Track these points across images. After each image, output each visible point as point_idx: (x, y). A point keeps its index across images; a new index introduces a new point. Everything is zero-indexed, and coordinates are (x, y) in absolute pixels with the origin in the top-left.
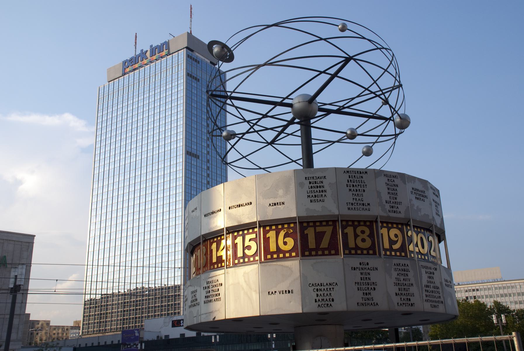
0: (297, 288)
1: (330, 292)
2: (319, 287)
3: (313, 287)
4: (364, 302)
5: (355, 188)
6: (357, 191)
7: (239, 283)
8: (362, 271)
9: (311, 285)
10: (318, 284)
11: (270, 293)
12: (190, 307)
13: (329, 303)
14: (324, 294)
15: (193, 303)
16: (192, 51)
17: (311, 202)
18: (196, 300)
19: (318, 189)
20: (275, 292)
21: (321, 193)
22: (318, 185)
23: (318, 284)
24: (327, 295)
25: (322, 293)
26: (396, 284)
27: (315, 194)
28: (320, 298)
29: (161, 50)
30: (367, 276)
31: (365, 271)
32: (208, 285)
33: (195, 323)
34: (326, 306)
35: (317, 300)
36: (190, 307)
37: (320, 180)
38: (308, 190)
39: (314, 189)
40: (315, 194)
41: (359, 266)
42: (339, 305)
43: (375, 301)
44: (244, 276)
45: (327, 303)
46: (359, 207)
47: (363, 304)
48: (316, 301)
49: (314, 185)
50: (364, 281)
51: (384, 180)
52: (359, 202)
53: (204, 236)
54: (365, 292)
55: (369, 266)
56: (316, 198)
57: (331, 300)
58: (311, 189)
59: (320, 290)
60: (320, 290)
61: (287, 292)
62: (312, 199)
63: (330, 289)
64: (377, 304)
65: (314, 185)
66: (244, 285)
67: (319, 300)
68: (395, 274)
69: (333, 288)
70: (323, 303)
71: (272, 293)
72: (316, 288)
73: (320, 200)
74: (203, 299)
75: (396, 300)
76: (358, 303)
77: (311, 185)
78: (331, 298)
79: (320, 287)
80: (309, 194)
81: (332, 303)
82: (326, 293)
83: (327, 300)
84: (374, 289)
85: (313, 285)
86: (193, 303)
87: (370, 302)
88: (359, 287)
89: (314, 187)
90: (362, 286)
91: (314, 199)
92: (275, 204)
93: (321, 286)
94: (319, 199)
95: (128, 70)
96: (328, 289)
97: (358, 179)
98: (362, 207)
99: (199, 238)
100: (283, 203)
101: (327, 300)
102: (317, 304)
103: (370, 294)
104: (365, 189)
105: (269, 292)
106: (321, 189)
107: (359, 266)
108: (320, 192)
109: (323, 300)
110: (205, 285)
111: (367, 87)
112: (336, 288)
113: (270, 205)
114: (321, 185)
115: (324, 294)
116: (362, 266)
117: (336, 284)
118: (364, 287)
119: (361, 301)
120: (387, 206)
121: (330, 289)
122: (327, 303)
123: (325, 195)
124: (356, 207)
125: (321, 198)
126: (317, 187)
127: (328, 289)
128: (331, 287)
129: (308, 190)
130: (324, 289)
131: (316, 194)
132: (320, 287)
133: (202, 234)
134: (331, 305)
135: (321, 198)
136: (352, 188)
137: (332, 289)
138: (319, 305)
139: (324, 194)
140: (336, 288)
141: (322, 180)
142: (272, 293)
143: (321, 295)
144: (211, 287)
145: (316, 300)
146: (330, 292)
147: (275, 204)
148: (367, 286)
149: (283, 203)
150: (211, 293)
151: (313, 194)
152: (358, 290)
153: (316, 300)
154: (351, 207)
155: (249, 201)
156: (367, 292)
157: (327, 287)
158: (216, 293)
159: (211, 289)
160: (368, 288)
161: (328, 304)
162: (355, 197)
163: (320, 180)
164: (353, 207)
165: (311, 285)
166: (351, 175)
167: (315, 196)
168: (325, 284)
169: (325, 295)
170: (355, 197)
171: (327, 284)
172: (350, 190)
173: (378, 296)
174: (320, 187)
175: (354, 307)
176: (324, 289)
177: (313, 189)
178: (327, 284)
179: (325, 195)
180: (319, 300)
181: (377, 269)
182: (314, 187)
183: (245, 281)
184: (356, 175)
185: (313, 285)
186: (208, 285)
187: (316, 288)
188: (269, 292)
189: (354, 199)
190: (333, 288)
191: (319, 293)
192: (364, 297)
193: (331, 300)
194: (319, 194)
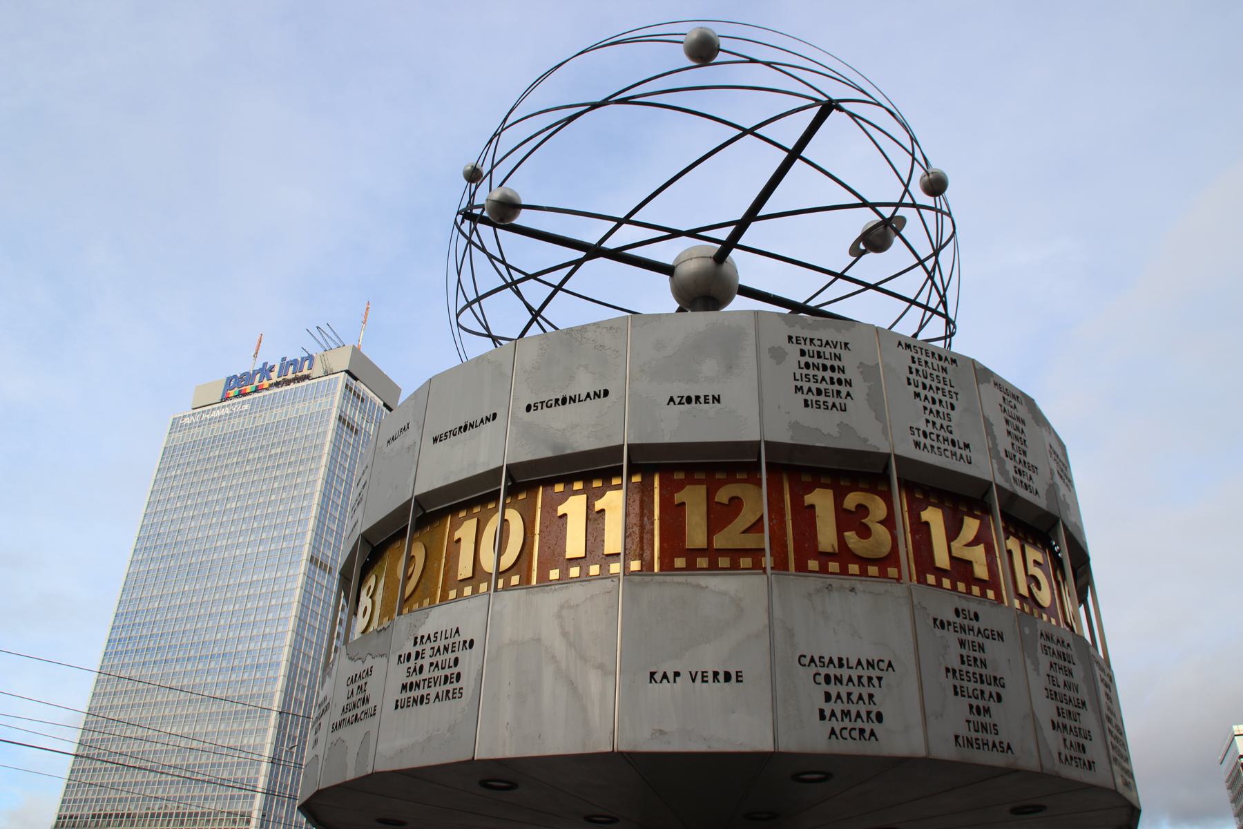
0: (754, 664)
1: (871, 690)
2: (832, 671)
3: (813, 669)
4: (973, 735)
5: (930, 394)
6: (934, 402)
7: (538, 640)
8: (963, 636)
9: (806, 661)
10: (831, 661)
11: (658, 677)
12: (337, 727)
13: (868, 727)
14: (849, 694)
15: (349, 714)
17: (806, 405)
18: (365, 700)
19: (828, 374)
20: (677, 674)
21: (836, 387)
22: (828, 363)
23: (831, 661)
24: (860, 697)
25: (843, 690)
26: (1052, 695)
27: (818, 385)
28: (838, 708)
29: (294, 373)
30: (977, 654)
31: (970, 637)
32: (419, 648)
33: (350, 775)
34: (856, 734)
35: (827, 714)
36: (337, 727)
37: (833, 351)
38: (798, 372)
39: (816, 372)
40: (818, 385)
41: (951, 617)
42: (902, 735)
43: (1003, 737)
44: (559, 616)
45: (859, 724)
46: (943, 447)
47: (969, 742)
48: (822, 717)
49: (816, 360)
50: (971, 669)
51: (991, 401)
52: (942, 433)
53: (421, 501)
54: (974, 702)
55: (980, 625)
56: (822, 398)
57: (873, 716)
58: (805, 371)
59: (839, 680)
60: (839, 680)
61: (721, 677)
62: (810, 397)
63: (870, 679)
64: (1009, 747)
65: (816, 360)
66: (559, 646)
67: (833, 714)
68: (1044, 661)
69: (880, 679)
70: (847, 723)
71: (665, 676)
72: (823, 671)
73: (834, 405)
74: (394, 693)
75: (1054, 740)
76: (957, 737)
77: (806, 359)
78: (874, 709)
79: (838, 672)
80: (799, 384)
81: (876, 726)
82: (856, 691)
83: (858, 715)
84: (999, 698)
85: (812, 660)
86: (349, 714)
87: (990, 738)
88: (958, 683)
89: (816, 367)
90: (965, 684)
91: (815, 398)
92: (689, 400)
93: (841, 665)
94: (830, 401)
95: (232, 393)
96: (865, 680)
97: (935, 373)
98: (950, 448)
99: (403, 509)
100: (717, 399)
101: (858, 715)
102: (827, 726)
103: (987, 710)
104: (954, 401)
105: (652, 674)
106: (836, 376)
107: (951, 617)
108: (832, 383)
109: (846, 714)
110: (410, 648)
111: (897, 201)
112: (888, 677)
113: (672, 399)
114: (836, 363)
115: (849, 694)
116: (959, 621)
117: (890, 665)
118: (971, 685)
119: (963, 731)
120: (1010, 465)
121: (870, 679)
122: (859, 724)
123: (848, 394)
124: (935, 444)
125: (837, 401)
126: (825, 368)
127: (865, 680)
128: (874, 673)
129: (798, 372)
130: (850, 679)
131: (823, 386)
132: (838, 672)
133: (416, 493)
134: (872, 733)
135: (837, 401)
136: (923, 393)
137: (875, 681)
138: (833, 732)
139: (844, 389)
140: (888, 677)
141: (838, 351)
142: (665, 676)
143: (839, 696)
144: (428, 652)
145: (822, 711)
146: (871, 690)
147: (689, 400)
148: (978, 686)
149: (717, 399)
150: (426, 674)
151: (814, 386)
152: (956, 694)
153: (822, 711)
154: (922, 440)
155: (600, 387)
156: (981, 703)
157: (860, 671)
158: (448, 672)
159: (426, 662)
160: (982, 692)
161: (862, 731)
162: (931, 418)
163: (833, 351)
164: (928, 442)
165: (804, 661)
166: (916, 356)
167: (819, 392)
168: (853, 663)
169: (854, 697)
170: (931, 418)
171: (859, 663)
172: (917, 395)
173: (1008, 721)
174: (833, 369)
175: (946, 751)
176: (850, 679)
177: (811, 372)
178: (859, 663)
179: (848, 394)
180: (833, 714)
181: (1001, 636)
182: (816, 367)
183: (565, 634)
184: (920, 368)
185: (812, 660)
186: (419, 648)
187: (823, 671)
188: (652, 674)
189: (927, 421)
190: (880, 679)
191: (833, 689)
192: (971, 718)
193: (873, 716)
194: (830, 387)
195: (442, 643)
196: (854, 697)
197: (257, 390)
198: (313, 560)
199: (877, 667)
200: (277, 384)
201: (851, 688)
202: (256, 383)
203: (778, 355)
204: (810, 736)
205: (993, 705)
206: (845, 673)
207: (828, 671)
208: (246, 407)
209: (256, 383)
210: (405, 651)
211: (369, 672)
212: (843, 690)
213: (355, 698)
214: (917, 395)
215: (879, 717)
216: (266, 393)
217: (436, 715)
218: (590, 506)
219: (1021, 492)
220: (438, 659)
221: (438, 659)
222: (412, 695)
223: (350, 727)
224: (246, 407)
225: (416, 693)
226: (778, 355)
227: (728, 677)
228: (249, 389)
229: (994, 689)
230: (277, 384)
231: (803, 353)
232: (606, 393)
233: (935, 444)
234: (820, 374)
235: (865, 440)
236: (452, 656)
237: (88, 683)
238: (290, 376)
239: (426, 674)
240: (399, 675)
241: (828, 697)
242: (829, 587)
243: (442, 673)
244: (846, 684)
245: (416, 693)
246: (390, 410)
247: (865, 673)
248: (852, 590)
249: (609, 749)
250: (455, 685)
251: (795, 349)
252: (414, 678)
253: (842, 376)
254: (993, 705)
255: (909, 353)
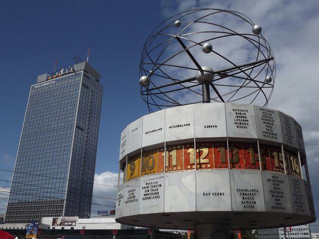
2: (244, 192)
3: (240, 192)
12: (126, 202)
13: (252, 205)
16: (87, 72)
28: (246, 201)
31: (275, 183)
34: (250, 207)
36: (126, 202)
48: (242, 203)
49: (240, 115)
58: (237, 118)
59: (246, 194)
60: (246, 194)
62: (238, 125)
65: (240, 115)
72: (242, 192)
80: (236, 122)
98: (272, 135)
100: (216, 126)
103: (279, 200)
106: (245, 119)
109: (247, 202)
110: (145, 186)
119: (274, 205)
124: (269, 135)
125: (245, 126)
128: (254, 193)
135: (245, 126)
139: (246, 123)
141: (245, 112)
149: (216, 126)
150: (150, 192)
154: (265, 134)
156: (278, 198)
168: (249, 190)
169: (249, 198)
177: (239, 118)
191: (245, 196)
195: (153, 185)
196: (249, 198)
197: (57, 77)
198: (77, 127)
199: (255, 192)
200: (63, 75)
201: (249, 196)
202: (57, 75)
203: (230, 114)
204: (239, 207)
205: (281, 199)
206: (247, 193)
207: (243, 193)
208: (54, 82)
209: (57, 75)
210: (144, 186)
211: (134, 190)
212: (247, 197)
213: (131, 196)
214: (264, 122)
215: (255, 203)
216: (60, 77)
217: (154, 202)
218: (186, 153)
219: (290, 145)
220: (153, 188)
221: (153, 188)
222: (147, 197)
223: (130, 203)
224: (54, 82)
225: (148, 196)
226: (230, 114)
227: (221, 194)
228: (55, 76)
229: (281, 195)
230: (63, 75)
231: (236, 113)
232: (189, 125)
233: (269, 135)
234: (241, 119)
235: (252, 136)
236: (157, 188)
237: (92, 209)
238: (67, 72)
239: (150, 192)
240: (143, 192)
241: (243, 198)
242: (243, 173)
243: (154, 192)
244: (247, 195)
245: (148, 196)
246: (98, 81)
247: (252, 193)
248: (249, 173)
249: (195, 211)
250: (158, 195)
251: (235, 112)
252: (147, 193)
253: (246, 119)
254: (281, 199)
255: (262, 111)
